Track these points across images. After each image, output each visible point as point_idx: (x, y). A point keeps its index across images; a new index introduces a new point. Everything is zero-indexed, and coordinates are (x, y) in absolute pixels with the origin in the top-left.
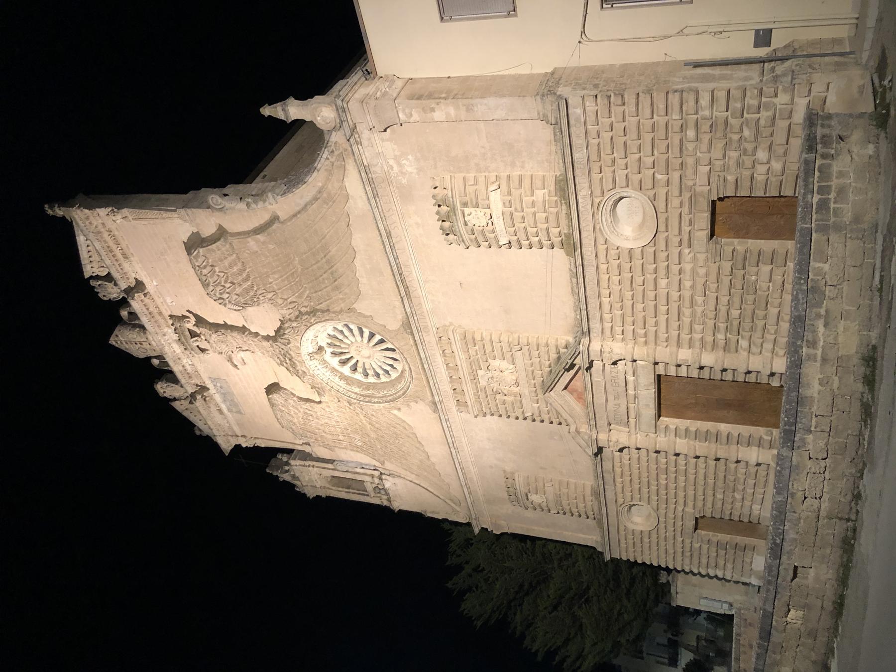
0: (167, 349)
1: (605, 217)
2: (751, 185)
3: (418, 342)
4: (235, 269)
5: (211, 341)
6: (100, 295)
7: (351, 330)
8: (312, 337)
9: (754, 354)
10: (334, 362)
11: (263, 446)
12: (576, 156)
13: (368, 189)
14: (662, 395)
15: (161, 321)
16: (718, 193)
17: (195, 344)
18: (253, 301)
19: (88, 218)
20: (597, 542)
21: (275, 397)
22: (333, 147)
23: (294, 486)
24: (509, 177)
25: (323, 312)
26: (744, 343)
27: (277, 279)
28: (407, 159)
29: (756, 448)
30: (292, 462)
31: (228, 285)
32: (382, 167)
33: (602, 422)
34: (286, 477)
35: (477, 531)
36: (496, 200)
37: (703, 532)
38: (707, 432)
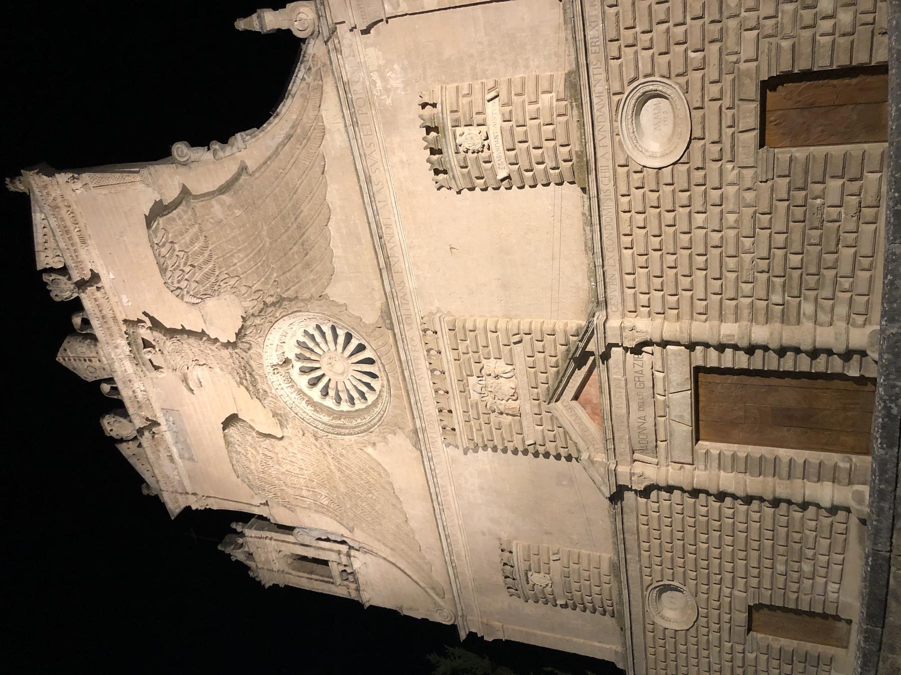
0: (116, 365)
1: (625, 126)
2: (813, 52)
3: (398, 336)
4: (197, 247)
5: (165, 352)
6: (52, 295)
7: (323, 334)
8: (277, 342)
9: (821, 325)
10: (303, 381)
11: (215, 508)
12: (590, 34)
13: (347, 112)
14: (701, 405)
15: (115, 328)
16: (769, 71)
17: (148, 356)
18: (212, 292)
19: (45, 187)
20: (616, 653)
21: (231, 431)
22: (310, 63)
23: (248, 568)
24: (510, 81)
25: (290, 300)
26: (808, 308)
27: (243, 259)
28: (393, 70)
29: (831, 483)
30: (247, 532)
31: (187, 269)
32: (364, 83)
33: (623, 447)
34: (238, 555)
35: (463, 635)
36: (494, 111)
37: (760, 635)
38: (761, 458)
